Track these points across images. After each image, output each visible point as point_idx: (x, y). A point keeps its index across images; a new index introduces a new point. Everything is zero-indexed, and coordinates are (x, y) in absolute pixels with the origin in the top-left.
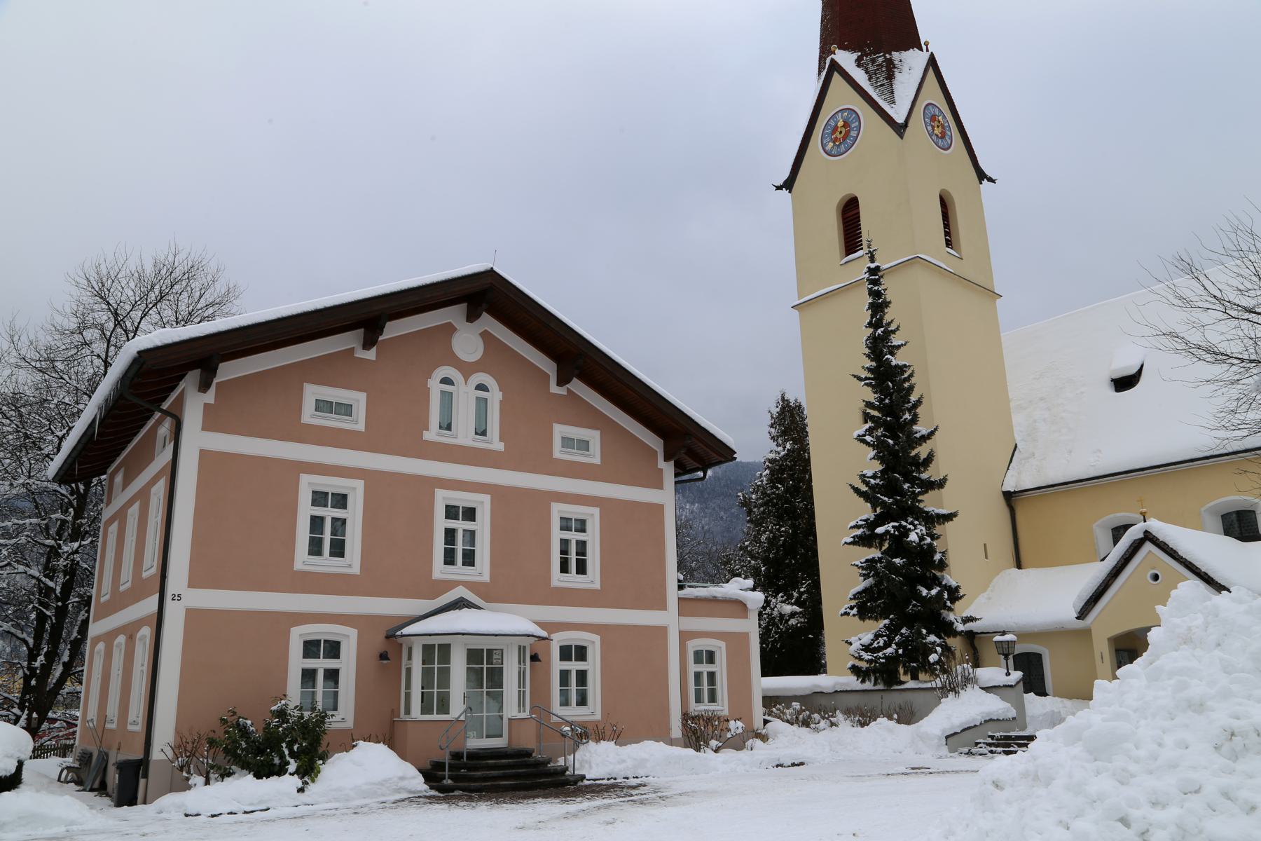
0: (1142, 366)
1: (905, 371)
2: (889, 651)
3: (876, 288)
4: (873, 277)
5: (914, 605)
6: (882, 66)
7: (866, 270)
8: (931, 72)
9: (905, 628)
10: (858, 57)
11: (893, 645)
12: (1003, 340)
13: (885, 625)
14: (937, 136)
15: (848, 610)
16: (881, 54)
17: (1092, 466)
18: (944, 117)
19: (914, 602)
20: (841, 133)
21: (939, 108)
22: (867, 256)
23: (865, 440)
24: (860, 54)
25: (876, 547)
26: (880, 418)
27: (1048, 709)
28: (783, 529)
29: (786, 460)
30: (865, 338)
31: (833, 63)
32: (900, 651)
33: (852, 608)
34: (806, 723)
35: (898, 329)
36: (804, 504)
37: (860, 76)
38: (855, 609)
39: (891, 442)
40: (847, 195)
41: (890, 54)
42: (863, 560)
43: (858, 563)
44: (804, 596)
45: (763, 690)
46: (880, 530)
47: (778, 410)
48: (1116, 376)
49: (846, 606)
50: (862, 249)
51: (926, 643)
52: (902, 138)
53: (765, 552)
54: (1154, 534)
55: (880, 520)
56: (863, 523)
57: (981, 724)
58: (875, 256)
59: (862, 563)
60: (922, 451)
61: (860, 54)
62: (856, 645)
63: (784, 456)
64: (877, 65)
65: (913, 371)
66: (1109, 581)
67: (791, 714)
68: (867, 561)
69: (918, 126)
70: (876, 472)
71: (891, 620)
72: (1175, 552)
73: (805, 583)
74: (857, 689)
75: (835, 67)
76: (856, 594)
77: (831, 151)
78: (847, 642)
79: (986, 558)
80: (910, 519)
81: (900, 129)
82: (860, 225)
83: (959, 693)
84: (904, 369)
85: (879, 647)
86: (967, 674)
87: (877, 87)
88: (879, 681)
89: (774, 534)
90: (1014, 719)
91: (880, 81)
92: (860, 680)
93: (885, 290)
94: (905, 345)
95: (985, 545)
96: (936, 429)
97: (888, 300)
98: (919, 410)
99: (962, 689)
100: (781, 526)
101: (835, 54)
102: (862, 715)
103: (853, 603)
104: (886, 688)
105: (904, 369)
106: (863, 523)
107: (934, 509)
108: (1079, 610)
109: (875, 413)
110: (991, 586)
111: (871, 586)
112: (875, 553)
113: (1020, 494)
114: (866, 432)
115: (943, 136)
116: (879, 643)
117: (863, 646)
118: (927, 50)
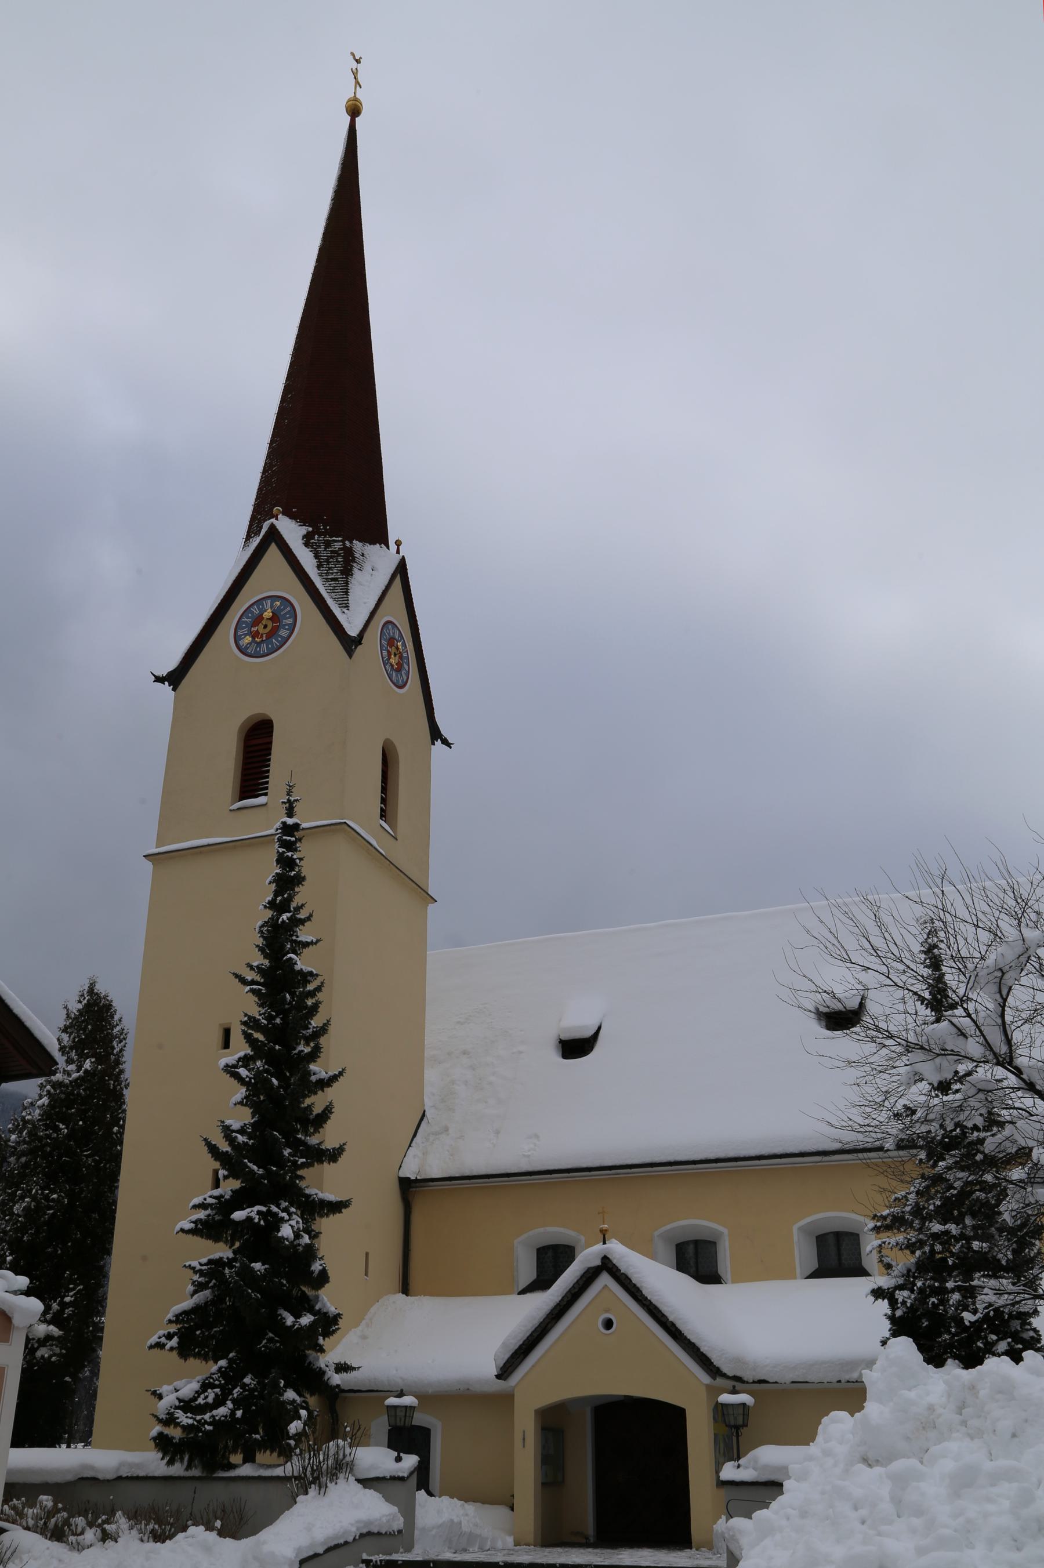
0: (599, 1028)
1: (309, 982)
2: (222, 1411)
3: (290, 854)
4: (288, 838)
5: (270, 1340)
6: (339, 555)
7: (278, 825)
8: (398, 581)
9: (250, 1376)
10: (308, 533)
11: (230, 1404)
12: (429, 959)
13: (221, 1368)
14: (392, 666)
15: (163, 1340)
16: (340, 539)
17: (524, 1155)
18: (404, 644)
19: (271, 1335)
20: (265, 627)
21: (399, 631)
22: (284, 806)
23: (238, 1073)
24: (310, 529)
25: (226, 1242)
26: (265, 1045)
27: (445, 1517)
28: (55, 1196)
29: (79, 1086)
30: (260, 923)
31: (273, 529)
32: (239, 1413)
33: (169, 1337)
34: (58, 1535)
35: (309, 918)
36: (94, 1161)
37: (306, 559)
38: (175, 1340)
39: (275, 1081)
40: (264, 714)
41: (351, 542)
42: (204, 1260)
43: (195, 1264)
44: (68, 1311)
45: (10, 1472)
46: (238, 1215)
47: (80, 1006)
48: (566, 1036)
49: (161, 1332)
50: (266, 794)
51: (284, 1402)
52: (350, 656)
53: (16, 1230)
54: (615, 1262)
55: (239, 1200)
56: (214, 1201)
57: (354, 1539)
58: (295, 809)
59: (201, 1265)
60: (317, 1102)
61: (310, 529)
62: (170, 1400)
63: (77, 1079)
64: (332, 552)
65: (322, 983)
66: (547, 1324)
67: (37, 1518)
68: (210, 1262)
69: (372, 647)
70: (245, 1125)
71: (231, 1362)
72: (638, 1290)
73: (73, 1289)
74: (156, 1474)
75: (274, 536)
76: (181, 1314)
77: (247, 648)
78: (154, 1393)
79: (366, 1274)
80: (284, 1204)
81: (350, 644)
82: (269, 760)
83: (326, 1487)
84: (309, 978)
85: (207, 1404)
86: (341, 1456)
87: (327, 580)
88: (196, 1462)
89: (38, 1203)
90: (400, 1532)
91: (332, 574)
92: (167, 1459)
93: (301, 859)
94: (316, 943)
95: (367, 1254)
96: (341, 1074)
97: (303, 875)
98: (323, 1040)
99: (331, 1480)
100: (53, 1192)
101: (277, 519)
102: (159, 1522)
103: (173, 1328)
104: (204, 1475)
105: (309, 978)
106: (214, 1201)
107: (317, 1191)
108: (502, 1365)
109: (259, 1036)
110: (366, 1317)
111: (206, 1303)
112: (223, 1251)
113: (422, 1184)
114: (238, 1061)
115: (399, 670)
116: (206, 1397)
117: (180, 1400)
118: (398, 552)
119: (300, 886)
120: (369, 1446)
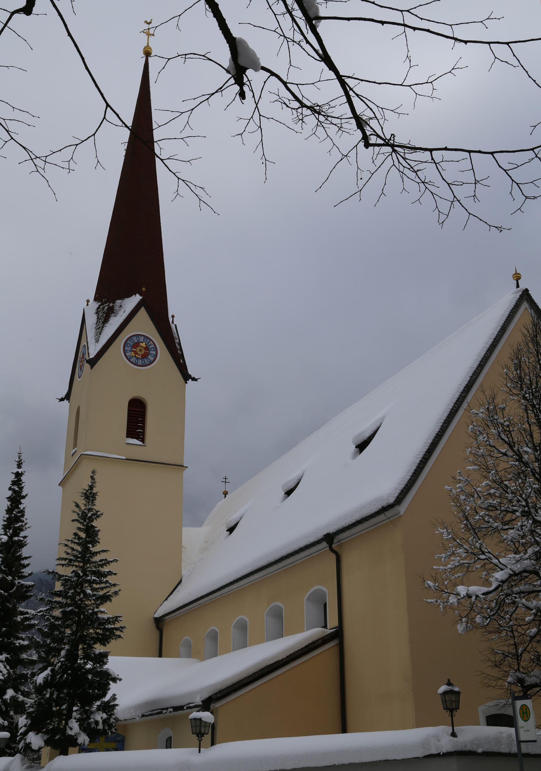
119: (22, 501)
120: (124, 750)
